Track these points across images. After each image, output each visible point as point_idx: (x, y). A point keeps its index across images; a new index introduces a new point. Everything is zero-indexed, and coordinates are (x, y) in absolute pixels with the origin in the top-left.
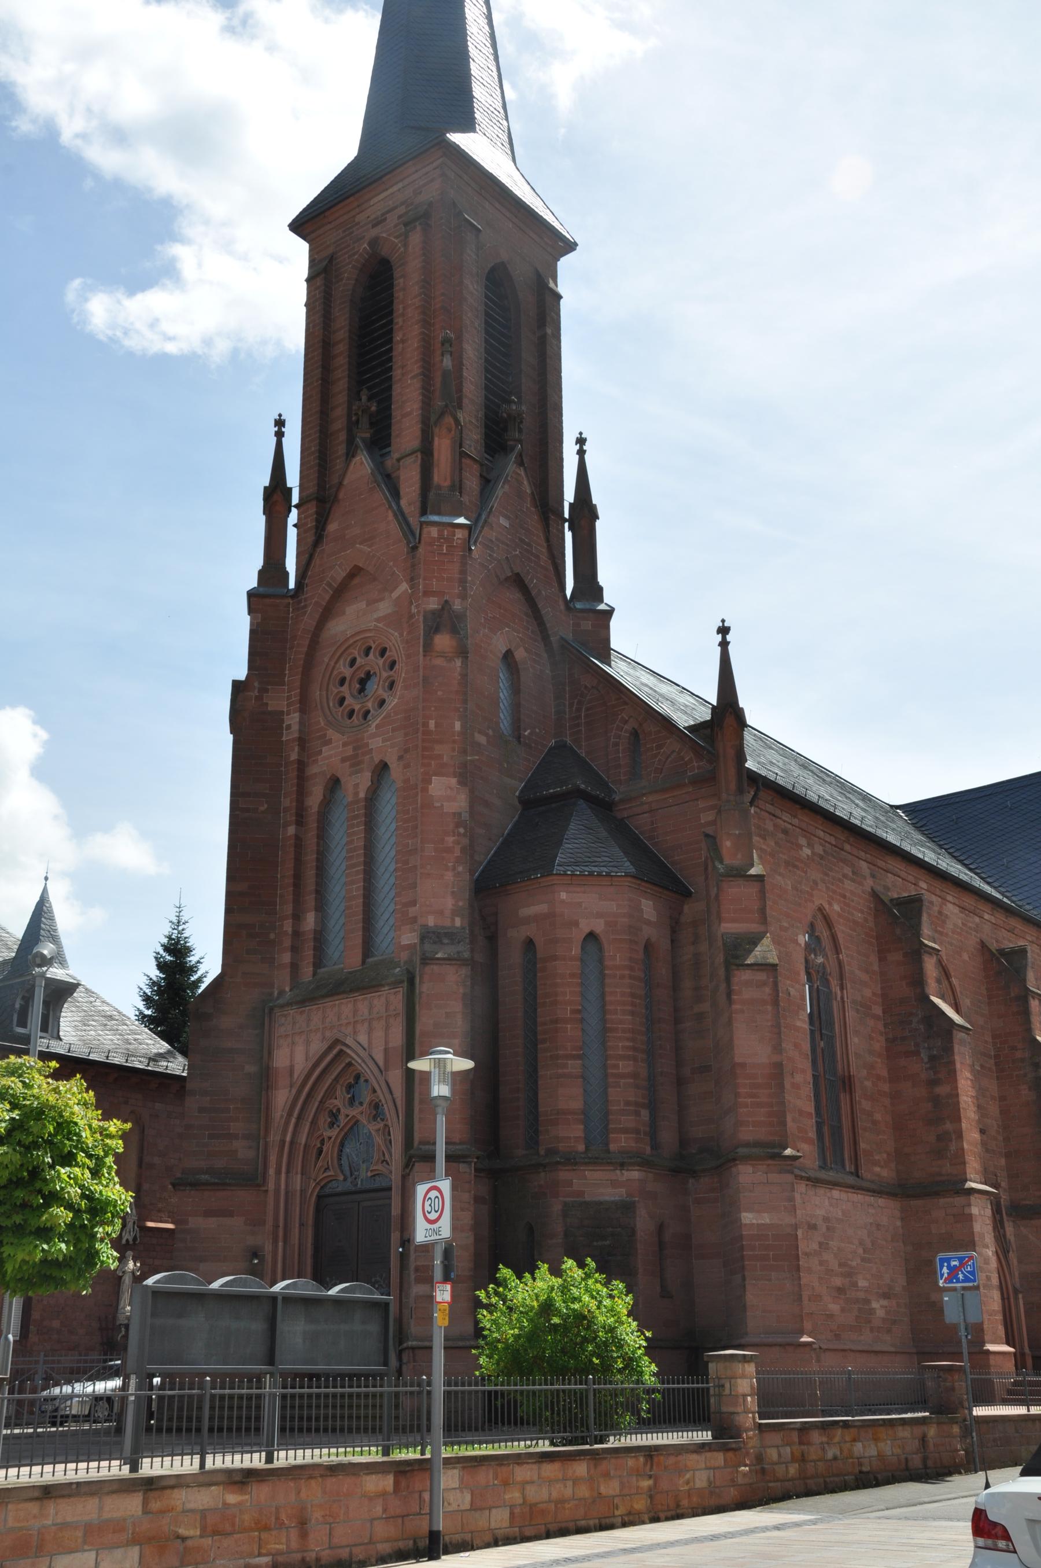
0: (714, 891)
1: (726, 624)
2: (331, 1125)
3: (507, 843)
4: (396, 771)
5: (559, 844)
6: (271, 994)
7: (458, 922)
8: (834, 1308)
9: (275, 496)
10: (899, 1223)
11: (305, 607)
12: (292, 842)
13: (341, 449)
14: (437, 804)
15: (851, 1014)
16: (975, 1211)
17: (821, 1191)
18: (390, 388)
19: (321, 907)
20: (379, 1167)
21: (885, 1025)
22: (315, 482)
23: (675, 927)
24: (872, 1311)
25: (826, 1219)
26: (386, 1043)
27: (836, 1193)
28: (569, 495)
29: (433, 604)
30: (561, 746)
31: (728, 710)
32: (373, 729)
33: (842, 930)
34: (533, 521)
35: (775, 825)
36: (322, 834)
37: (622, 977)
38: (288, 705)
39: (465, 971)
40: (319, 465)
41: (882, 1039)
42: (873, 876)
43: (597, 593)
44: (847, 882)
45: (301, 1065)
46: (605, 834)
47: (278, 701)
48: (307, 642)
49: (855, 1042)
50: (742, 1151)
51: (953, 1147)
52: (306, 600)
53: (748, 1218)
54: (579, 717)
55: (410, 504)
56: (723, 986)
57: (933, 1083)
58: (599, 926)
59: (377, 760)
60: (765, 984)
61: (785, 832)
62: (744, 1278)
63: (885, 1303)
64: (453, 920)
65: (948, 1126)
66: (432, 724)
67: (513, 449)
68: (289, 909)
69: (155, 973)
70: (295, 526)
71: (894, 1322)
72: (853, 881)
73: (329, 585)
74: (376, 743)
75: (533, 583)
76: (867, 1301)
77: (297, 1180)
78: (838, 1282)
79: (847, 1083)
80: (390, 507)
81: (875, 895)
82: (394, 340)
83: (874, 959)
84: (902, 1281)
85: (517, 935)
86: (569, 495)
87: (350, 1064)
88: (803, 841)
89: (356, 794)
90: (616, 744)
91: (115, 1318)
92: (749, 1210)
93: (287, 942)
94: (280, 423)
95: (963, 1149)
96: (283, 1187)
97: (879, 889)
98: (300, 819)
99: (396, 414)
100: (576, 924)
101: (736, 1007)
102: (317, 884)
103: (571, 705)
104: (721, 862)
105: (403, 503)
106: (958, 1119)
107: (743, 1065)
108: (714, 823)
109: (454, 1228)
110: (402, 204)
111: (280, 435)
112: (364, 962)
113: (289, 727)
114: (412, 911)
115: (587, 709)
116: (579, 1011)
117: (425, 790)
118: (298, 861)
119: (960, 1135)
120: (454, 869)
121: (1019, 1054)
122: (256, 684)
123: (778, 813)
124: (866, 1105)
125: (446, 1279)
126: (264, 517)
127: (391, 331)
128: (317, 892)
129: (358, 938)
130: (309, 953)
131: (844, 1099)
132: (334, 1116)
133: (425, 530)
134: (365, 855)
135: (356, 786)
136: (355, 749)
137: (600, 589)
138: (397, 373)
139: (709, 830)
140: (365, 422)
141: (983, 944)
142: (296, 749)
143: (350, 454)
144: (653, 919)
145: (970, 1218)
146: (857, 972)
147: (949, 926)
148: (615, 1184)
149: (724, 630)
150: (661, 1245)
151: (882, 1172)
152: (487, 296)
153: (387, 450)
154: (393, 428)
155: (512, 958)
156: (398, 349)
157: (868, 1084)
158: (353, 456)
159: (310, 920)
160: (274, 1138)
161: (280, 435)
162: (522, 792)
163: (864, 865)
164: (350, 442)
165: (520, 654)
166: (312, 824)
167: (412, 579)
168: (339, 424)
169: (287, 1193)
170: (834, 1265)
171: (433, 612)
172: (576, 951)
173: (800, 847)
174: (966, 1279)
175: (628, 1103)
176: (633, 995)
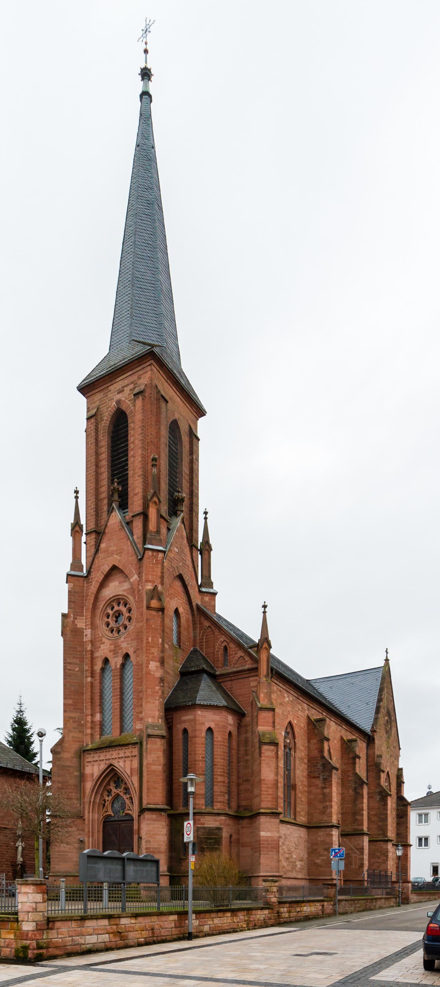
0: (255, 714)
1: (266, 604)
2: (108, 796)
3: (175, 690)
4: (133, 657)
5: (197, 692)
6: (83, 745)
7: (160, 720)
8: (285, 864)
9: (76, 528)
10: (307, 836)
11: (92, 582)
12: (90, 684)
13: (105, 508)
14: (152, 673)
15: (297, 762)
16: (334, 833)
17: (284, 825)
18: (127, 479)
19: (102, 712)
20: (128, 812)
21: (308, 767)
22: (94, 523)
23: (239, 726)
24: (296, 866)
25: (285, 835)
26: (131, 766)
27: (288, 826)
28: (200, 540)
29: (149, 587)
30: (195, 651)
31: (265, 641)
32: (122, 639)
33: (296, 730)
34: (187, 550)
35: (277, 689)
36: (101, 682)
37: (220, 745)
38: (86, 626)
39: (163, 741)
40: (96, 515)
41: (307, 771)
42: (308, 710)
43: (210, 585)
44: (299, 712)
45: (96, 773)
46: (214, 688)
47: (81, 623)
48: (93, 599)
49: (298, 772)
50: (262, 811)
51: (328, 811)
52: (92, 579)
53: (262, 834)
54: (202, 639)
55: (138, 538)
56: (257, 750)
57: (323, 788)
58: (212, 725)
59: (124, 653)
60: (273, 750)
61: (280, 691)
62: (260, 854)
63: (300, 863)
64: (158, 721)
65: (328, 804)
66: (150, 639)
67: (180, 515)
68: (89, 712)
69: (11, 732)
70: (85, 543)
71: (303, 869)
72: (301, 711)
73: (102, 573)
74: (124, 645)
75: (186, 578)
76: (295, 862)
77: (96, 816)
78: (287, 856)
79: (294, 787)
80: (129, 539)
81: (308, 717)
82: (129, 455)
83: (306, 741)
84: (306, 856)
85: (180, 727)
86: (200, 540)
87: (116, 774)
88: (286, 695)
89: (116, 666)
90: (218, 651)
91: (16, 862)
92: (263, 831)
93: (89, 725)
94: (77, 492)
95: (332, 812)
96: (91, 817)
97: (310, 715)
98: (92, 675)
99: (131, 494)
100: (204, 724)
101: (262, 758)
102: (100, 702)
103: (200, 633)
104: (259, 702)
105: (135, 537)
106: (331, 801)
107: (264, 780)
108: (256, 686)
109: (194, 838)
110: (132, 383)
111: (77, 497)
112: (120, 735)
113: (86, 635)
114: (140, 716)
115: (207, 636)
116: (204, 757)
117: (147, 667)
118: (92, 693)
119: (331, 807)
120: (159, 700)
121: (350, 778)
122: (72, 615)
123: (278, 683)
124: (299, 795)
125: (193, 854)
126: (71, 538)
127: (127, 450)
128: (100, 705)
129: (118, 725)
130: (98, 729)
131: (293, 792)
132: (109, 792)
133: (146, 552)
134: (120, 692)
135: (116, 663)
136: (115, 647)
137: (212, 583)
138: (130, 473)
139: (254, 689)
140: (116, 497)
141: (342, 737)
142: (90, 645)
143: (110, 511)
144: (232, 723)
145: (332, 835)
146: (300, 746)
147: (331, 730)
148: (215, 821)
149: (265, 607)
150: (230, 842)
151: (302, 819)
152: (169, 437)
153: (126, 510)
154: (129, 500)
155: (179, 736)
156: (131, 460)
157: (301, 787)
158: (112, 512)
159: (98, 717)
160: (87, 799)
161: (77, 497)
162: (181, 669)
163: (305, 705)
164: (110, 505)
165: (181, 610)
166: (97, 677)
167: (139, 574)
168: (104, 495)
169: (92, 820)
170: (286, 850)
171: (150, 590)
172: (204, 734)
173: (285, 697)
174: (340, 856)
175: (221, 792)
176: (224, 752)
